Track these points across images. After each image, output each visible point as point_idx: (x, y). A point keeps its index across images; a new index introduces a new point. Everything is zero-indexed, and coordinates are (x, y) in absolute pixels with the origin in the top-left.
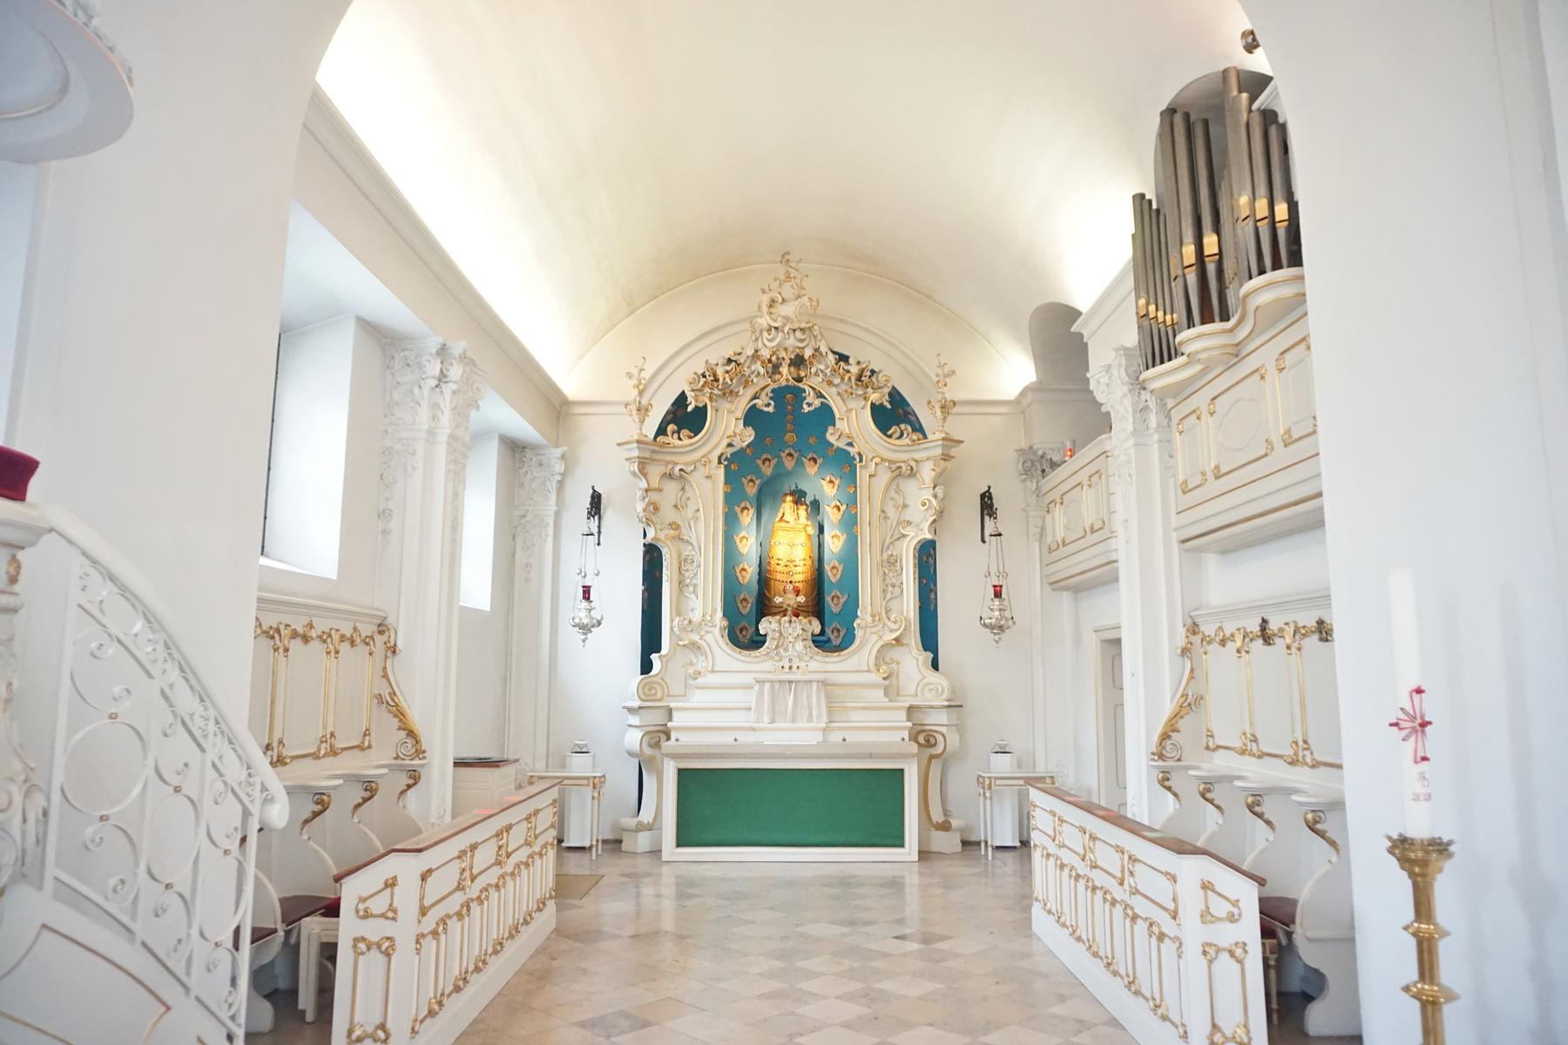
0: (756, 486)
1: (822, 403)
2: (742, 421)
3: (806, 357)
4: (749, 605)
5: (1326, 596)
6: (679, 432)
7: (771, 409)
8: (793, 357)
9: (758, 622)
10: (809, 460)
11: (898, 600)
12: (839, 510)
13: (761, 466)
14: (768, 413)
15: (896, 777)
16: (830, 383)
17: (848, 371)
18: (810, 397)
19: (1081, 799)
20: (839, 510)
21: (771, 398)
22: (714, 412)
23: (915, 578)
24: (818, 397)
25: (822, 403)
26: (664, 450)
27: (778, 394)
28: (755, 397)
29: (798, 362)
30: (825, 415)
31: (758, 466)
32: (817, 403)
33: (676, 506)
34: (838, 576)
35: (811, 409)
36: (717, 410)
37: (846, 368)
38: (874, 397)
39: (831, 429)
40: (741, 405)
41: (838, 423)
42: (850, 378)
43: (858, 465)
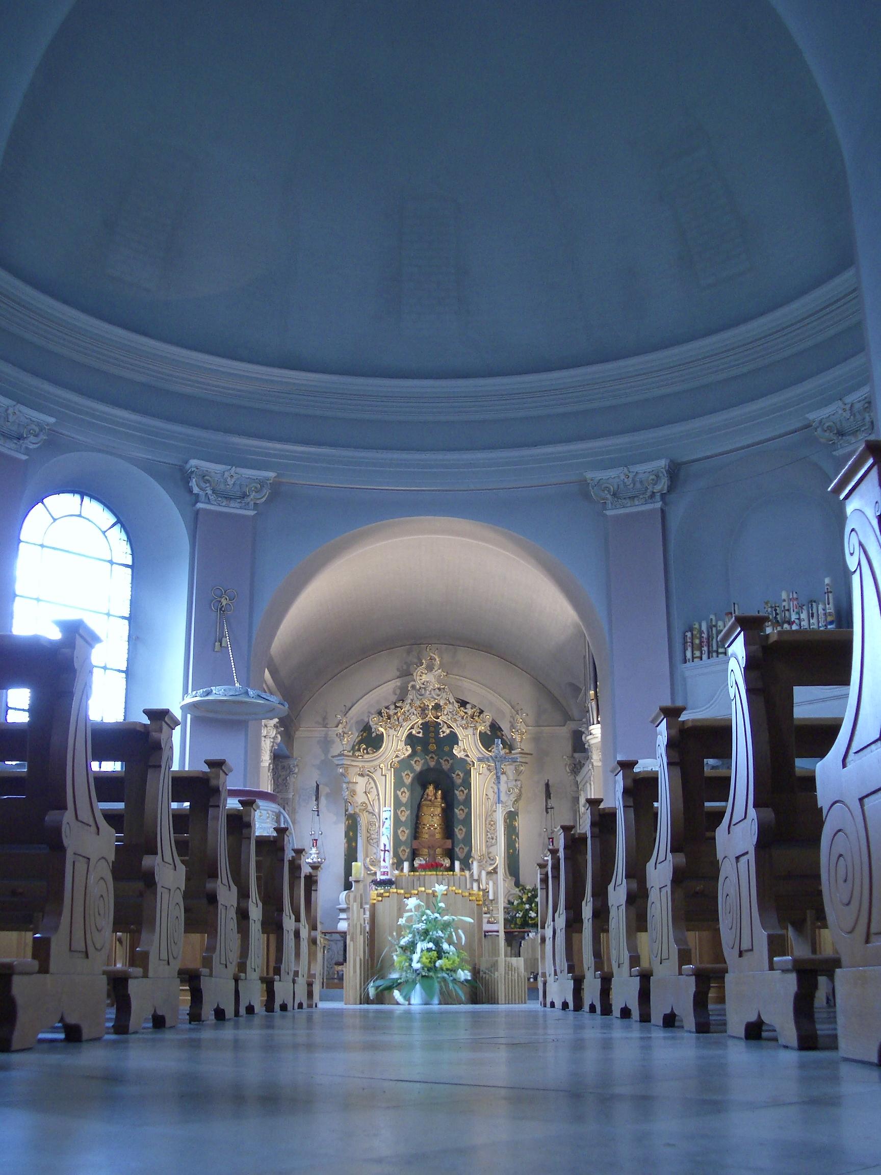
0: (410, 778)
1: (451, 731)
2: (403, 742)
3: (441, 704)
4: (407, 854)
5: (520, 955)
6: (367, 749)
7: (420, 735)
8: (433, 705)
9: (413, 860)
10: (445, 761)
11: (496, 846)
12: (463, 811)
13: (414, 765)
14: (418, 737)
15: (655, 780)
16: (456, 720)
17: (466, 713)
18: (445, 728)
19: (384, 986)
20: (463, 793)
21: (421, 728)
22: (387, 737)
23: (504, 834)
24: (448, 728)
25: (451, 731)
26: (357, 760)
27: (426, 726)
28: (412, 728)
29: (437, 707)
30: (453, 739)
31: (412, 765)
32: (448, 731)
33: (365, 792)
34: (463, 835)
35: (445, 734)
36: (389, 736)
37: (465, 711)
38: (481, 728)
39: (456, 746)
40: (403, 733)
41: (460, 743)
42: (467, 717)
43: (472, 768)
